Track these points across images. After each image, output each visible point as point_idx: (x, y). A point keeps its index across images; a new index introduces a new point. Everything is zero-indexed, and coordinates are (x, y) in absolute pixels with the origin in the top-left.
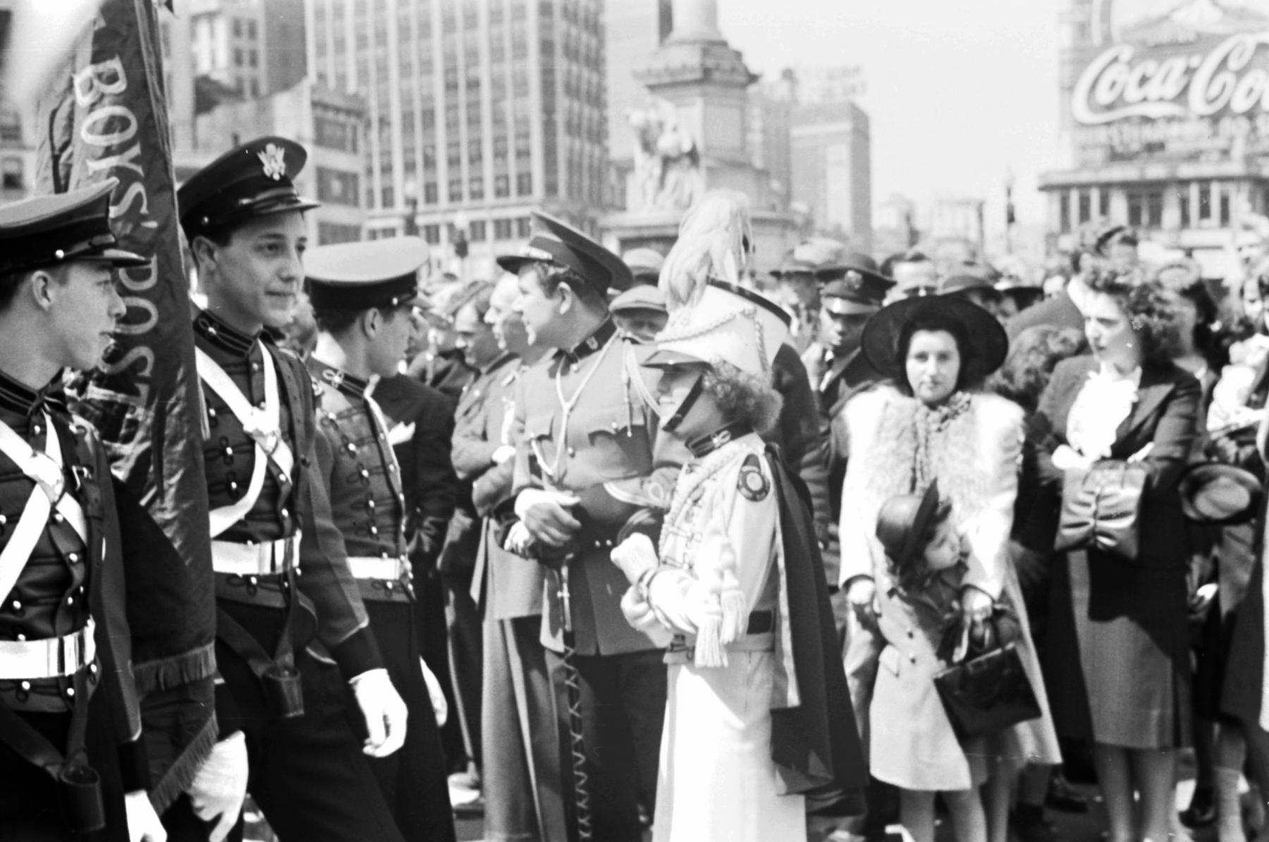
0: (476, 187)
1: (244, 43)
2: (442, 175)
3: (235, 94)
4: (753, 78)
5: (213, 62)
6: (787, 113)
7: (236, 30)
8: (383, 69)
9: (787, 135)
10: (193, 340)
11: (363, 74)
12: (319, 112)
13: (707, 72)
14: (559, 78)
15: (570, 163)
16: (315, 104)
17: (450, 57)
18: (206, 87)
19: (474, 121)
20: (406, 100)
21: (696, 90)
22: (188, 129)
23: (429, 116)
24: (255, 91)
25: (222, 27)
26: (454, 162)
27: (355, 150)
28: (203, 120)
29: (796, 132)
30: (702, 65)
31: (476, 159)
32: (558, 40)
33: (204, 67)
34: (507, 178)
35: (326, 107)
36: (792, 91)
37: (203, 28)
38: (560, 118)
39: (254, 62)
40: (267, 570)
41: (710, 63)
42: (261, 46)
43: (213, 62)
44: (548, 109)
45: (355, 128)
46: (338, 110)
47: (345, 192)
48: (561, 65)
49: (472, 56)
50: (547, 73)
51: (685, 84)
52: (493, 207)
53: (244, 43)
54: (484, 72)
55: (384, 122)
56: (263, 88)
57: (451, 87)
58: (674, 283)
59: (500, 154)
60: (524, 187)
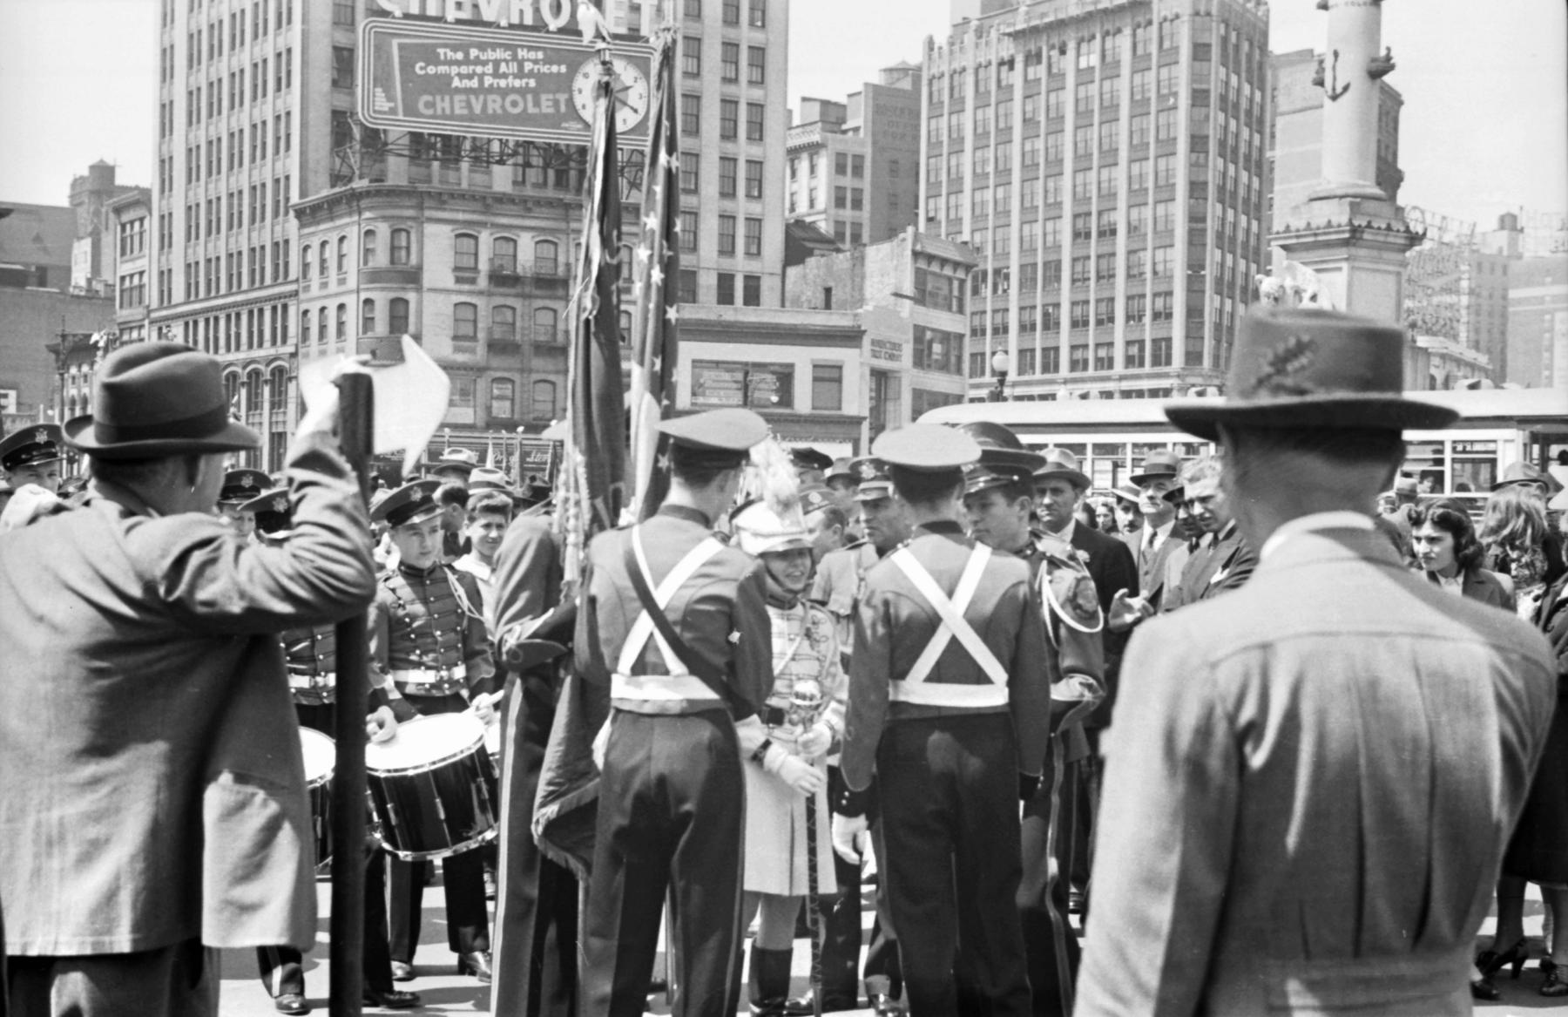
0: (1102, 353)
1: (848, 181)
2: (1064, 339)
3: (832, 243)
4: (1414, 239)
5: (812, 204)
6: (1505, 269)
7: (840, 169)
8: (1003, 213)
9: (1505, 298)
10: (360, 993)
11: (978, 218)
12: (922, 264)
13: (1355, 231)
14: (1211, 226)
15: (1218, 327)
16: (916, 255)
17: (1080, 199)
18: (799, 233)
19: (1105, 276)
20: (1027, 249)
21: (1343, 253)
22: (777, 281)
23: (1053, 269)
24: (856, 238)
25: (824, 163)
26: (1078, 324)
27: (961, 310)
28: (792, 272)
29: (1513, 294)
30: (1350, 223)
31: (1106, 320)
32: (1212, 179)
33: (802, 208)
34: (1141, 343)
35: (931, 258)
36: (1513, 243)
37: (803, 165)
38: (1209, 273)
39: (857, 204)
40: (803, 889)
41: (1360, 221)
42: (866, 184)
43: (812, 204)
44: (1195, 267)
45: (962, 282)
46: (944, 262)
47: (946, 354)
48: (1213, 209)
49: (1109, 196)
50: (1196, 218)
51: (1328, 245)
52: (1122, 378)
53: (848, 181)
54: (1120, 218)
55: (1001, 274)
56: (865, 238)
57: (1080, 235)
58: (13, 216)
59: (1133, 317)
60: (1162, 354)
